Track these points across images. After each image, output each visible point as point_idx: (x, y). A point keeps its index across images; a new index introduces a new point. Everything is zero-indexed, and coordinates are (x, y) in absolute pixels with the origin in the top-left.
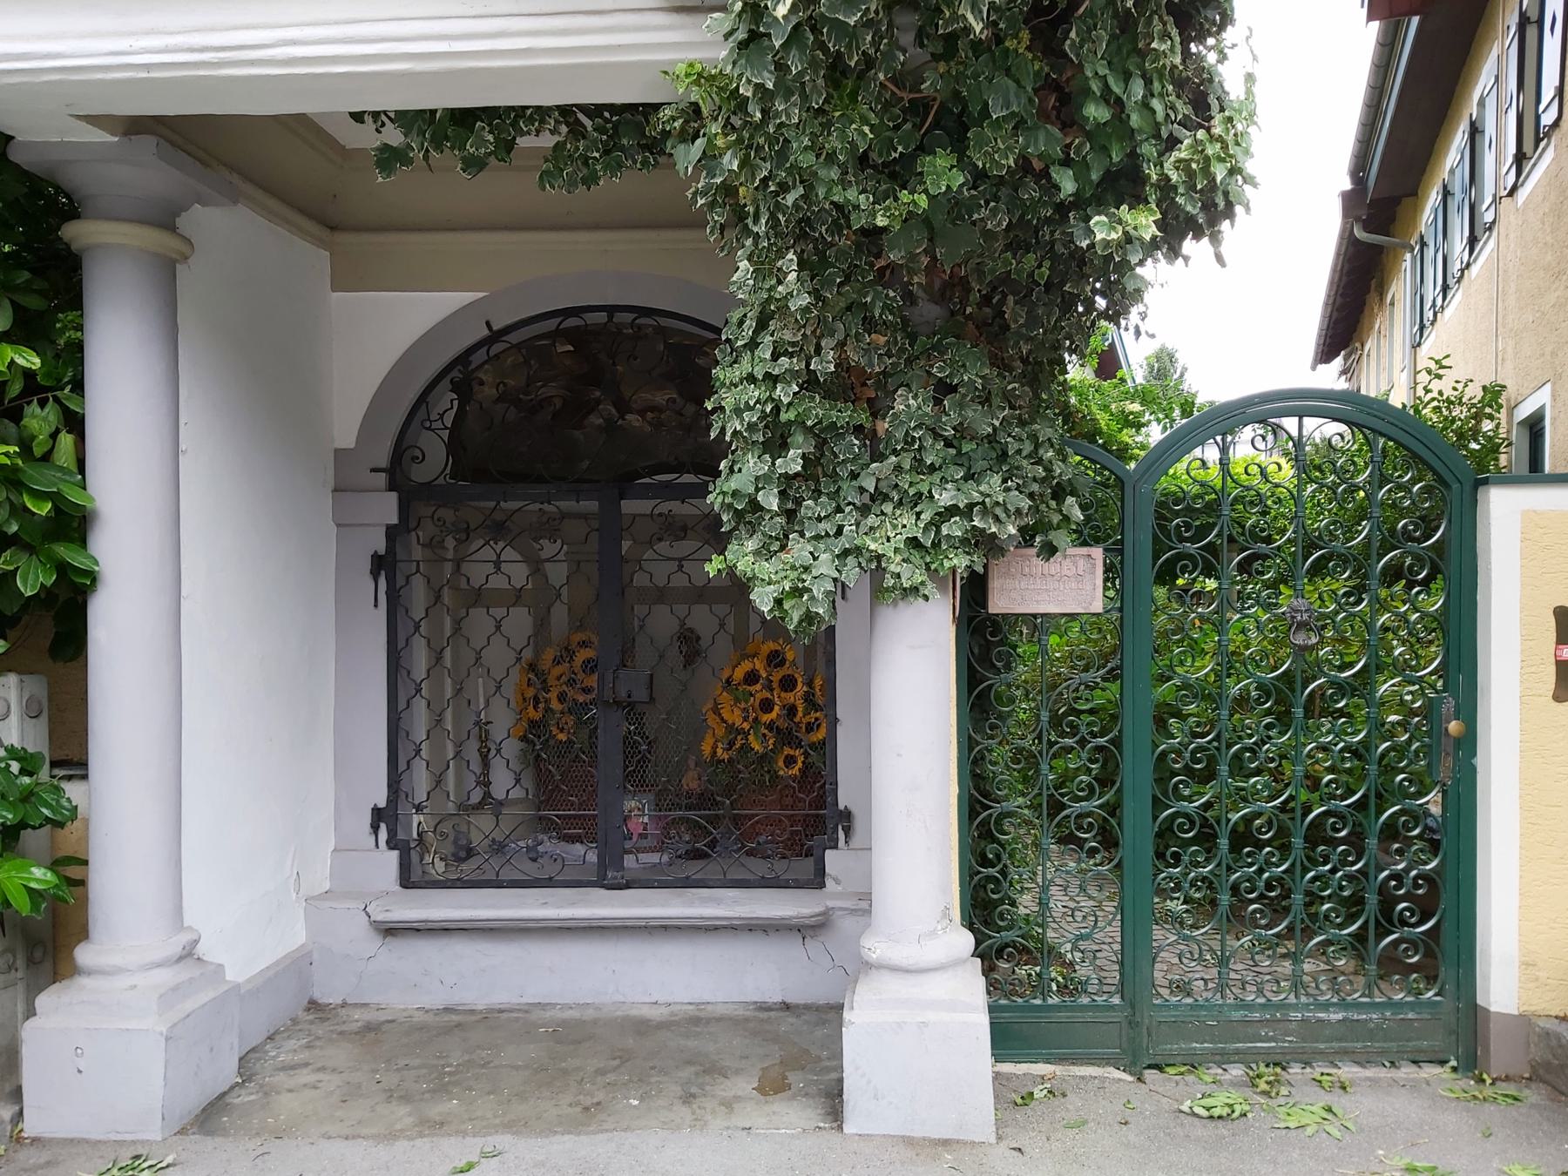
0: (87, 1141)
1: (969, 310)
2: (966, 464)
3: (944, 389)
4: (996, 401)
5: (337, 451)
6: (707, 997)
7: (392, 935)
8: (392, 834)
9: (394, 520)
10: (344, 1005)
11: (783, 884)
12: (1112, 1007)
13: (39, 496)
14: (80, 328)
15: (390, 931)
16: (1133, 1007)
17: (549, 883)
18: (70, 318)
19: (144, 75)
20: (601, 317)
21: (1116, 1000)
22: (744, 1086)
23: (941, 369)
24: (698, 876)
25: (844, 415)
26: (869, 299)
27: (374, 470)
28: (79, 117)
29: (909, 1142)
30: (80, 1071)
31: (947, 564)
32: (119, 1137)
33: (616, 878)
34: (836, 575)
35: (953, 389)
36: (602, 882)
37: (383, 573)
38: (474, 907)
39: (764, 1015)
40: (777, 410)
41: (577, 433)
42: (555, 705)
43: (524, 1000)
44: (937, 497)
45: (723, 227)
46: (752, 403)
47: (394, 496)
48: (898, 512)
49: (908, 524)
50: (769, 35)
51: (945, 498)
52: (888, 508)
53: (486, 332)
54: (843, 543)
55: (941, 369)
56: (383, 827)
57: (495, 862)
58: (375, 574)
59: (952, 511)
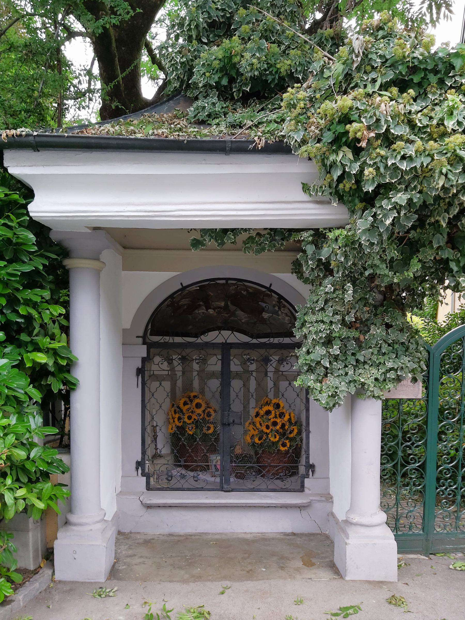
0: (78, 582)
1: (393, 297)
2: (395, 352)
3: (388, 326)
4: (405, 330)
5: (123, 330)
6: (264, 531)
7: (150, 508)
8: (143, 470)
9: (145, 355)
10: (131, 533)
11: (289, 490)
12: (420, 535)
13: (62, 358)
14: (68, 296)
15: (149, 507)
16: (427, 534)
17: (202, 489)
18: (65, 292)
19: (127, 219)
20: (224, 282)
21: (421, 532)
22: (299, 564)
23: (388, 320)
24: (258, 487)
25: (354, 333)
26: (368, 297)
27: (137, 337)
28: (86, 227)
29: (369, 582)
30: (75, 559)
31: (387, 387)
32: (89, 581)
33: (228, 488)
34: (347, 390)
35: (391, 326)
36: (222, 489)
37: (140, 375)
38: (195, 499)
39: (288, 537)
40: (331, 333)
41: (190, 317)
42: (186, 420)
43: (198, 531)
44: (387, 364)
45: (312, 269)
46: (322, 330)
47: (145, 346)
48: (371, 369)
49: (375, 373)
50: (378, 228)
51: (390, 365)
52: (367, 367)
53: (181, 287)
54: (348, 378)
55: (388, 320)
56: (140, 468)
57: (183, 481)
58: (138, 375)
59: (391, 369)
